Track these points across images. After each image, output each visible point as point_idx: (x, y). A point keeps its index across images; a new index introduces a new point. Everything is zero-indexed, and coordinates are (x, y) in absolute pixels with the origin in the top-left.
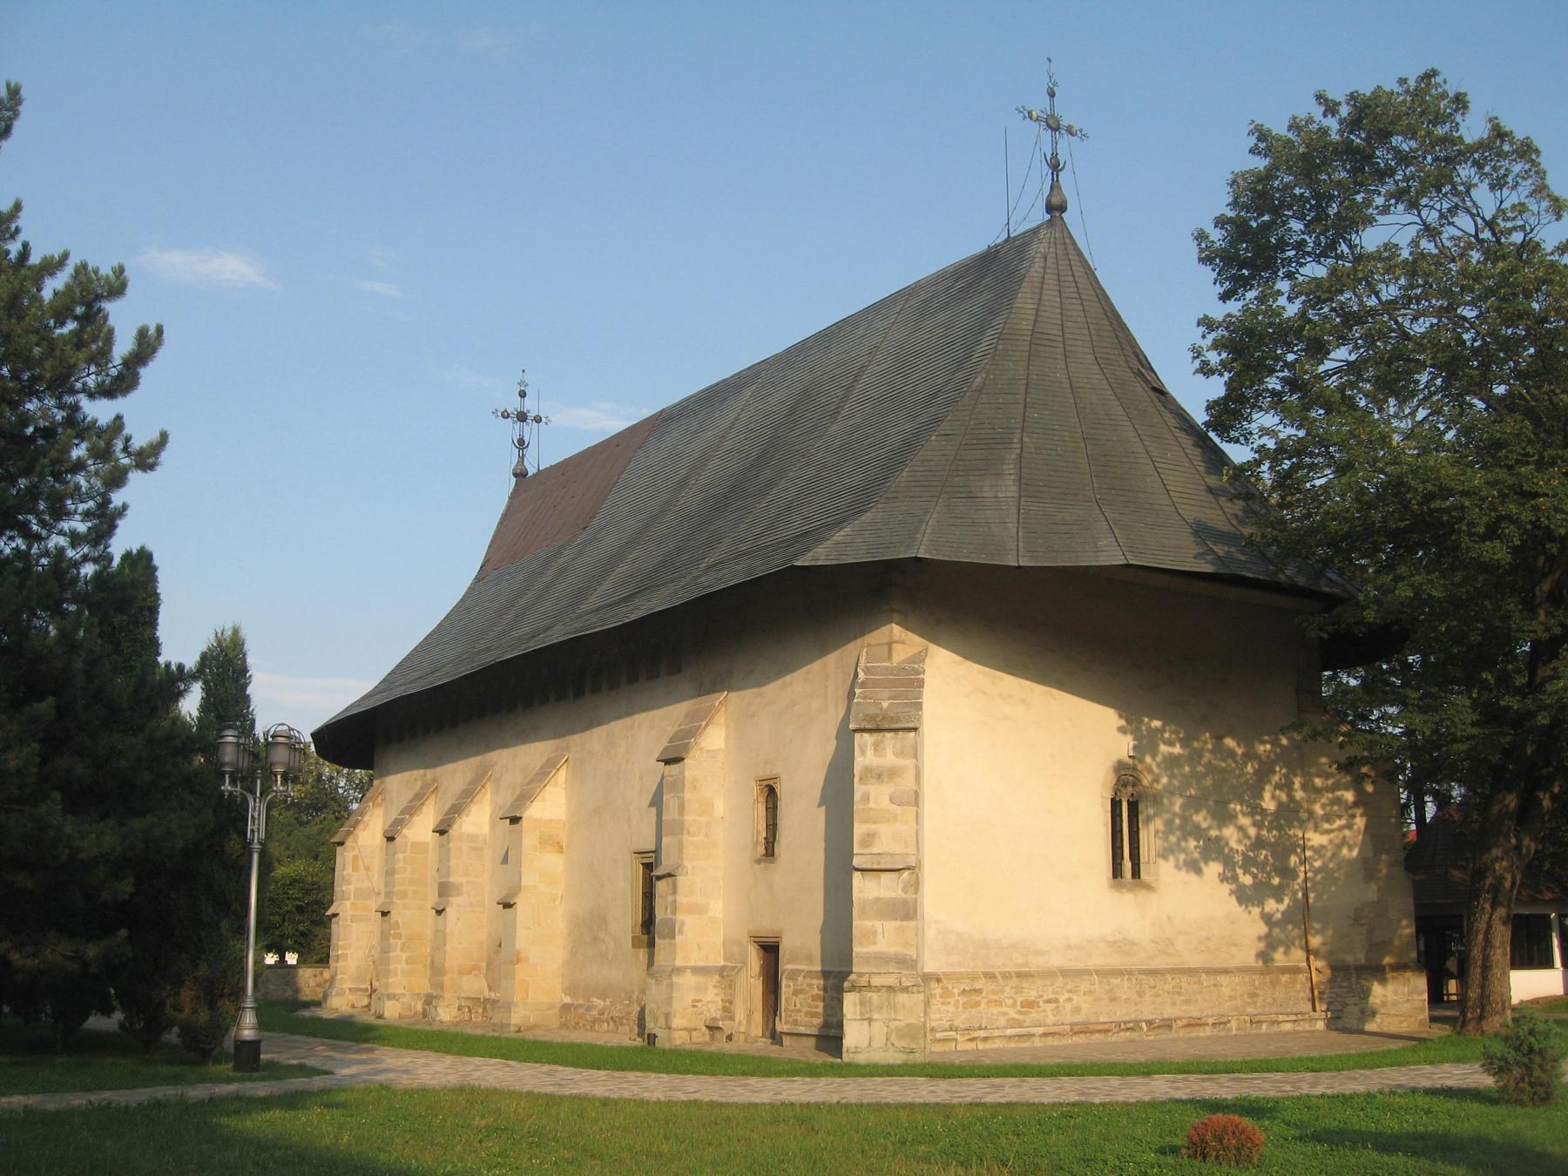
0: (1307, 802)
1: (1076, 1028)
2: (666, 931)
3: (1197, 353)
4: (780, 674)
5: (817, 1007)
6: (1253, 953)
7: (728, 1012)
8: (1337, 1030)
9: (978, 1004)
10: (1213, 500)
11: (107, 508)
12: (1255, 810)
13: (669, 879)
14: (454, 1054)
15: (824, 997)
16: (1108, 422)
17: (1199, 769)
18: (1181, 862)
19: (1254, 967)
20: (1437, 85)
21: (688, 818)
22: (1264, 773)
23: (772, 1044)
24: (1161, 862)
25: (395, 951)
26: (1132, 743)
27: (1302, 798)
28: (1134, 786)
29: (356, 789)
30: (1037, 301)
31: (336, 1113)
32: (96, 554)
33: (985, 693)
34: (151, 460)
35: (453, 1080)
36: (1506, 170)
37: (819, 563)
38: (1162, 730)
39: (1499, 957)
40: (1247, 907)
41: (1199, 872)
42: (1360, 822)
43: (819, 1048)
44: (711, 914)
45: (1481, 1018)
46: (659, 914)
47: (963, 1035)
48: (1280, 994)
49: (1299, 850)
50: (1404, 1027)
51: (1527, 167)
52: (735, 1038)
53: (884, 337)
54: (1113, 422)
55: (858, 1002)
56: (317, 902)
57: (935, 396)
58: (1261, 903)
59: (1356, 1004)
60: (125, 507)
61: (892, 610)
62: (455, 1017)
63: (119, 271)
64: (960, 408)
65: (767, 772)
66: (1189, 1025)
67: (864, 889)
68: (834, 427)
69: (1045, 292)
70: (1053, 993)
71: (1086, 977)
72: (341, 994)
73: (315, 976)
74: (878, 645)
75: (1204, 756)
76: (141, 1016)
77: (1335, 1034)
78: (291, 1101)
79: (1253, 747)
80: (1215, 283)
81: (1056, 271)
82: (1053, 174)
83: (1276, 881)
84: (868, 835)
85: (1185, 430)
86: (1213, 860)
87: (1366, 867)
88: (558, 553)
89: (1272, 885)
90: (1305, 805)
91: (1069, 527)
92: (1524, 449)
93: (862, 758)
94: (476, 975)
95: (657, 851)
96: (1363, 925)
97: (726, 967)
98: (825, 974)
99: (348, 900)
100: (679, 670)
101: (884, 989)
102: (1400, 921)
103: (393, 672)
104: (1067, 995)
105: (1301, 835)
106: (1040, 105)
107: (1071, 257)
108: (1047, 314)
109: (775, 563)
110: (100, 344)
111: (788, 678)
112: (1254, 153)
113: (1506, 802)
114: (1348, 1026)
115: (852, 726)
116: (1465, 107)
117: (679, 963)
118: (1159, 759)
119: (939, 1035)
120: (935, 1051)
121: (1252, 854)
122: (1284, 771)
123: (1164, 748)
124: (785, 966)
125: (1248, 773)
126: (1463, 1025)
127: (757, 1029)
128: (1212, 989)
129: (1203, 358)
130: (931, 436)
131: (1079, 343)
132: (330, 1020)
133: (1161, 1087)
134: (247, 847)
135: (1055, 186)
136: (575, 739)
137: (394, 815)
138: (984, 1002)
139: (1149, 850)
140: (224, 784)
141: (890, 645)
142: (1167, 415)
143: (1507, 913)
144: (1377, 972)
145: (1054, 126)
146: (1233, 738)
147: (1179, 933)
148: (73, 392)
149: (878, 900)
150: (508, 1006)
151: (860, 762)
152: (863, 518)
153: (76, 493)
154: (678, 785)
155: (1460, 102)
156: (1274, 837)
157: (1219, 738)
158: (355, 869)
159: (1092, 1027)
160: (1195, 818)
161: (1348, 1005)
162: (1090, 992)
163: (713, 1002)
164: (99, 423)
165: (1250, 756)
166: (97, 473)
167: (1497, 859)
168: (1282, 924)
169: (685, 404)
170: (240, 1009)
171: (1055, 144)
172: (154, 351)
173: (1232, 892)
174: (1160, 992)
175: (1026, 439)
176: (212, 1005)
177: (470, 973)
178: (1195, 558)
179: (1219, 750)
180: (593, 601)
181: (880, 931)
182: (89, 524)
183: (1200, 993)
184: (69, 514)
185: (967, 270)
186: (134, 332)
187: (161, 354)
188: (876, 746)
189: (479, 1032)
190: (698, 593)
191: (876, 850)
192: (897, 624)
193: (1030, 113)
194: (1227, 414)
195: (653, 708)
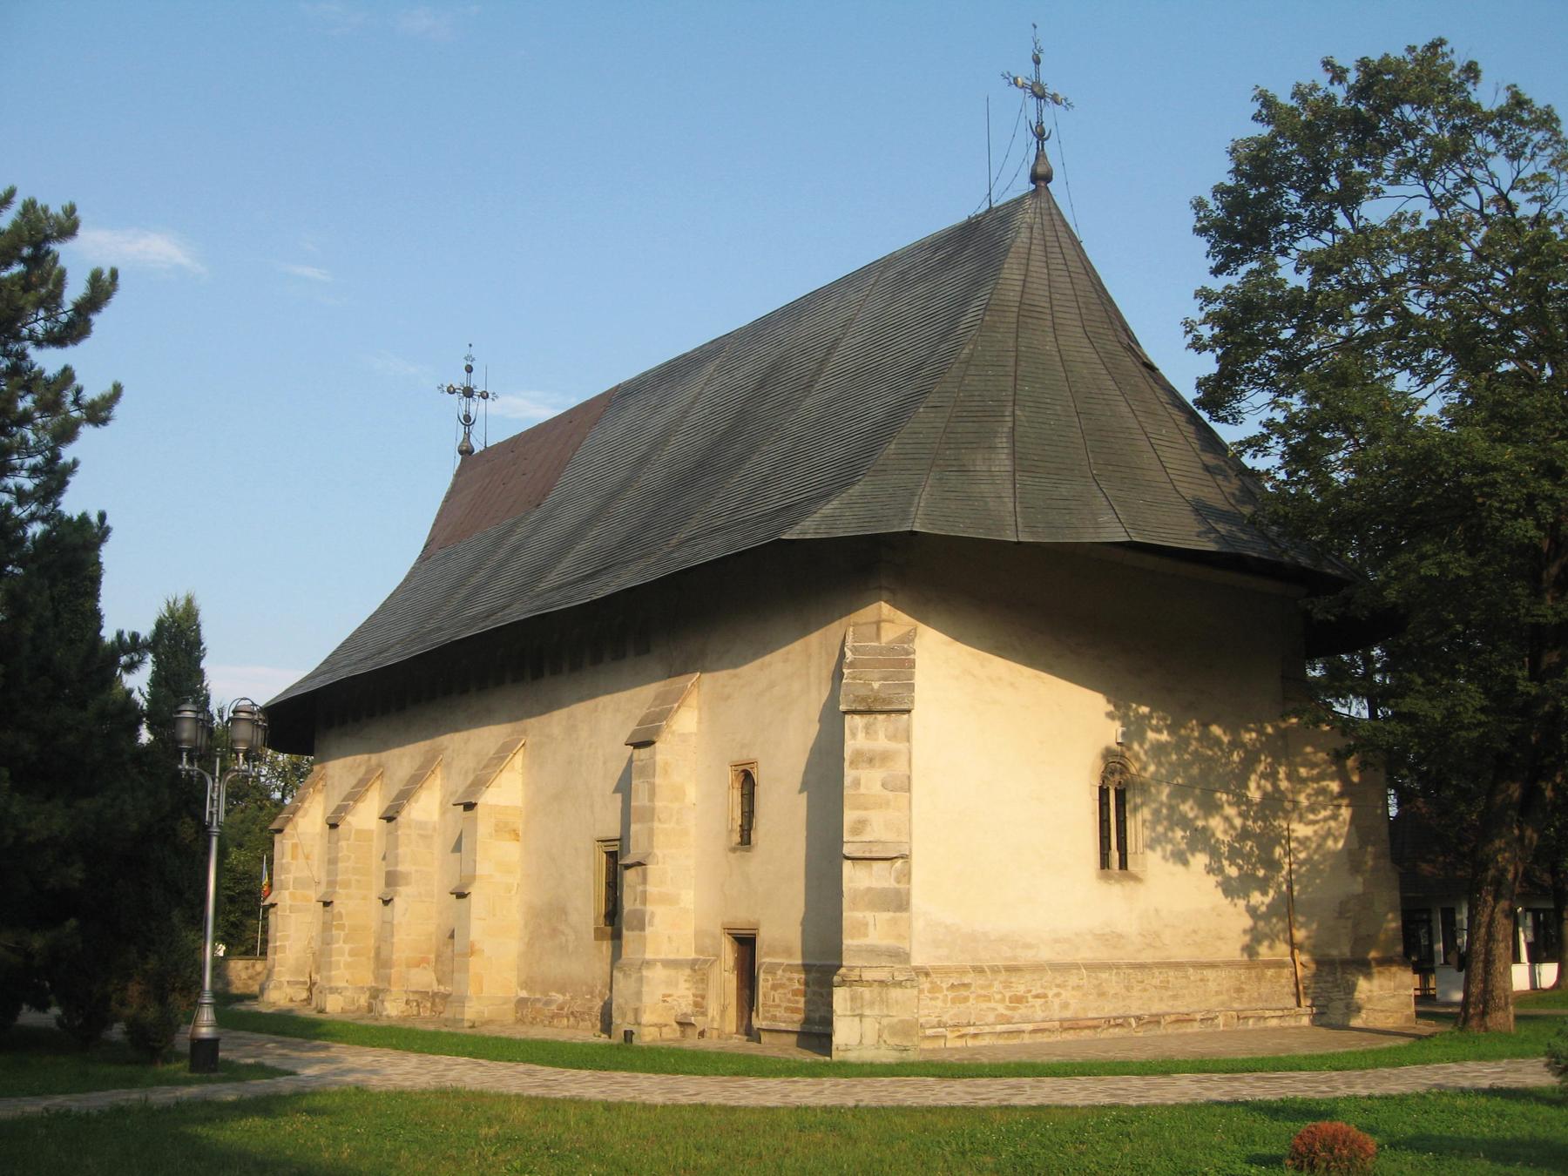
0: (1292, 792)
1: (1066, 1025)
3: (1189, 327)
4: (757, 655)
5: (797, 1002)
6: (1239, 946)
7: (700, 1006)
8: (1321, 1025)
9: (966, 999)
10: (1209, 478)
11: (56, 464)
12: (1241, 800)
13: (639, 868)
14: (415, 1051)
15: (805, 992)
17: (1186, 756)
18: (1168, 853)
19: (1240, 961)
20: (1444, 55)
21: (659, 804)
23: (748, 1040)
24: (1149, 852)
25: (338, 942)
26: (1120, 730)
27: (1287, 789)
28: (1121, 773)
29: (279, 776)
30: (1023, 272)
31: (324, 1121)
32: (45, 513)
33: (974, 676)
34: (103, 414)
36: (1527, 138)
37: (808, 537)
39: (1502, 951)
40: (1232, 899)
41: (1185, 863)
42: (1345, 813)
43: (800, 1044)
44: (682, 905)
45: (1484, 1014)
46: (628, 904)
47: (952, 1031)
48: (1265, 989)
49: (1283, 842)
50: (1389, 1023)
51: (1547, 136)
52: (707, 1035)
54: (1106, 397)
55: (848, 996)
56: (249, 892)
57: (919, 367)
58: (1246, 896)
59: (1341, 999)
60: (75, 463)
61: (880, 588)
62: (403, 1012)
63: (71, 211)
64: (949, 380)
65: (744, 756)
66: (1177, 1021)
67: (854, 878)
68: (809, 400)
69: (1031, 263)
70: (1042, 987)
71: (1075, 971)
72: (279, 987)
73: (247, 968)
74: (865, 624)
75: (1191, 744)
76: (81, 1012)
77: (1323, 1030)
78: (266, 1106)
79: (1239, 734)
80: (1207, 256)
81: (1043, 243)
82: (1038, 143)
83: (1261, 873)
84: (859, 822)
85: (1178, 407)
86: (1200, 851)
87: (1352, 859)
88: (510, 531)
89: (1258, 877)
90: (1290, 796)
91: (1067, 502)
92: (1553, 424)
93: (853, 742)
94: (425, 968)
95: (624, 839)
96: (1348, 918)
97: (698, 959)
98: (807, 968)
100: (648, 651)
101: (876, 984)
102: (1386, 914)
103: (335, 653)
104: (1055, 990)
105: (1285, 826)
106: (1025, 72)
108: (1035, 286)
109: (759, 537)
110: (51, 287)
111: (768, 658)
113: (1510, 792)
114: (1333, 1022)
115: (843, 708)
116: (1476, 77)
117: (649, 956)
118: (1147, 746)
119: (929, 1032)
120: (920, 1049)
121: (1237, 845)
122: (1269, 760)
123: (1151, 735)
124: (763, 959)
126: (1466, 1020)
127: (731, 1023)
128: (1199, 983)
129: (1196, 333)
130: (918, 407)
132: (266, 1014)
133: (1184, 1089)
134: (203, 830)
135: (1040, 155)
136: (533, 722)
137: (336, 801)
138: (972, 997)
139: (1136, 840)
140: (181, 764)
141: (878, 623)
142: (1160, 392)
143: (1510, 905)
144: (1363, 966)
145: (1039, 94)
146: (1220, 726)
147: (1166, 926)
148: (18, 338)
149: (869, 889)
150: (462, 1000)
151: (851, 745)
153: (24, 448)
154: (649, 770)
155: (1472, 71)
156: (1260, 827)
157: (1205, 725)
159: (1082, 1023)
162: (1078, 987)
163: (683, 997)
164: (46, 374)
165: (1236, 744)
166: (44, 427)
168: (1266, 917)
170: (196, 1005)
171: (1040, 112)
172: (108, 295)
173: (1218, 884)
174: (1148, 986)
175: (1018, 413)
177: (418, 966)
179: (1206, 738)
180: (553, 579)
181: (871, 922)
182: (37, 481)
184: (14, 470)
186: (88, 275)
187: (116, 300)
188: (867, 728)
189: (431, 1028)
190: (673, 569)
192: (886, 602)
193: (1015, 79)
194: (1218, 393)
195: (618, 690)
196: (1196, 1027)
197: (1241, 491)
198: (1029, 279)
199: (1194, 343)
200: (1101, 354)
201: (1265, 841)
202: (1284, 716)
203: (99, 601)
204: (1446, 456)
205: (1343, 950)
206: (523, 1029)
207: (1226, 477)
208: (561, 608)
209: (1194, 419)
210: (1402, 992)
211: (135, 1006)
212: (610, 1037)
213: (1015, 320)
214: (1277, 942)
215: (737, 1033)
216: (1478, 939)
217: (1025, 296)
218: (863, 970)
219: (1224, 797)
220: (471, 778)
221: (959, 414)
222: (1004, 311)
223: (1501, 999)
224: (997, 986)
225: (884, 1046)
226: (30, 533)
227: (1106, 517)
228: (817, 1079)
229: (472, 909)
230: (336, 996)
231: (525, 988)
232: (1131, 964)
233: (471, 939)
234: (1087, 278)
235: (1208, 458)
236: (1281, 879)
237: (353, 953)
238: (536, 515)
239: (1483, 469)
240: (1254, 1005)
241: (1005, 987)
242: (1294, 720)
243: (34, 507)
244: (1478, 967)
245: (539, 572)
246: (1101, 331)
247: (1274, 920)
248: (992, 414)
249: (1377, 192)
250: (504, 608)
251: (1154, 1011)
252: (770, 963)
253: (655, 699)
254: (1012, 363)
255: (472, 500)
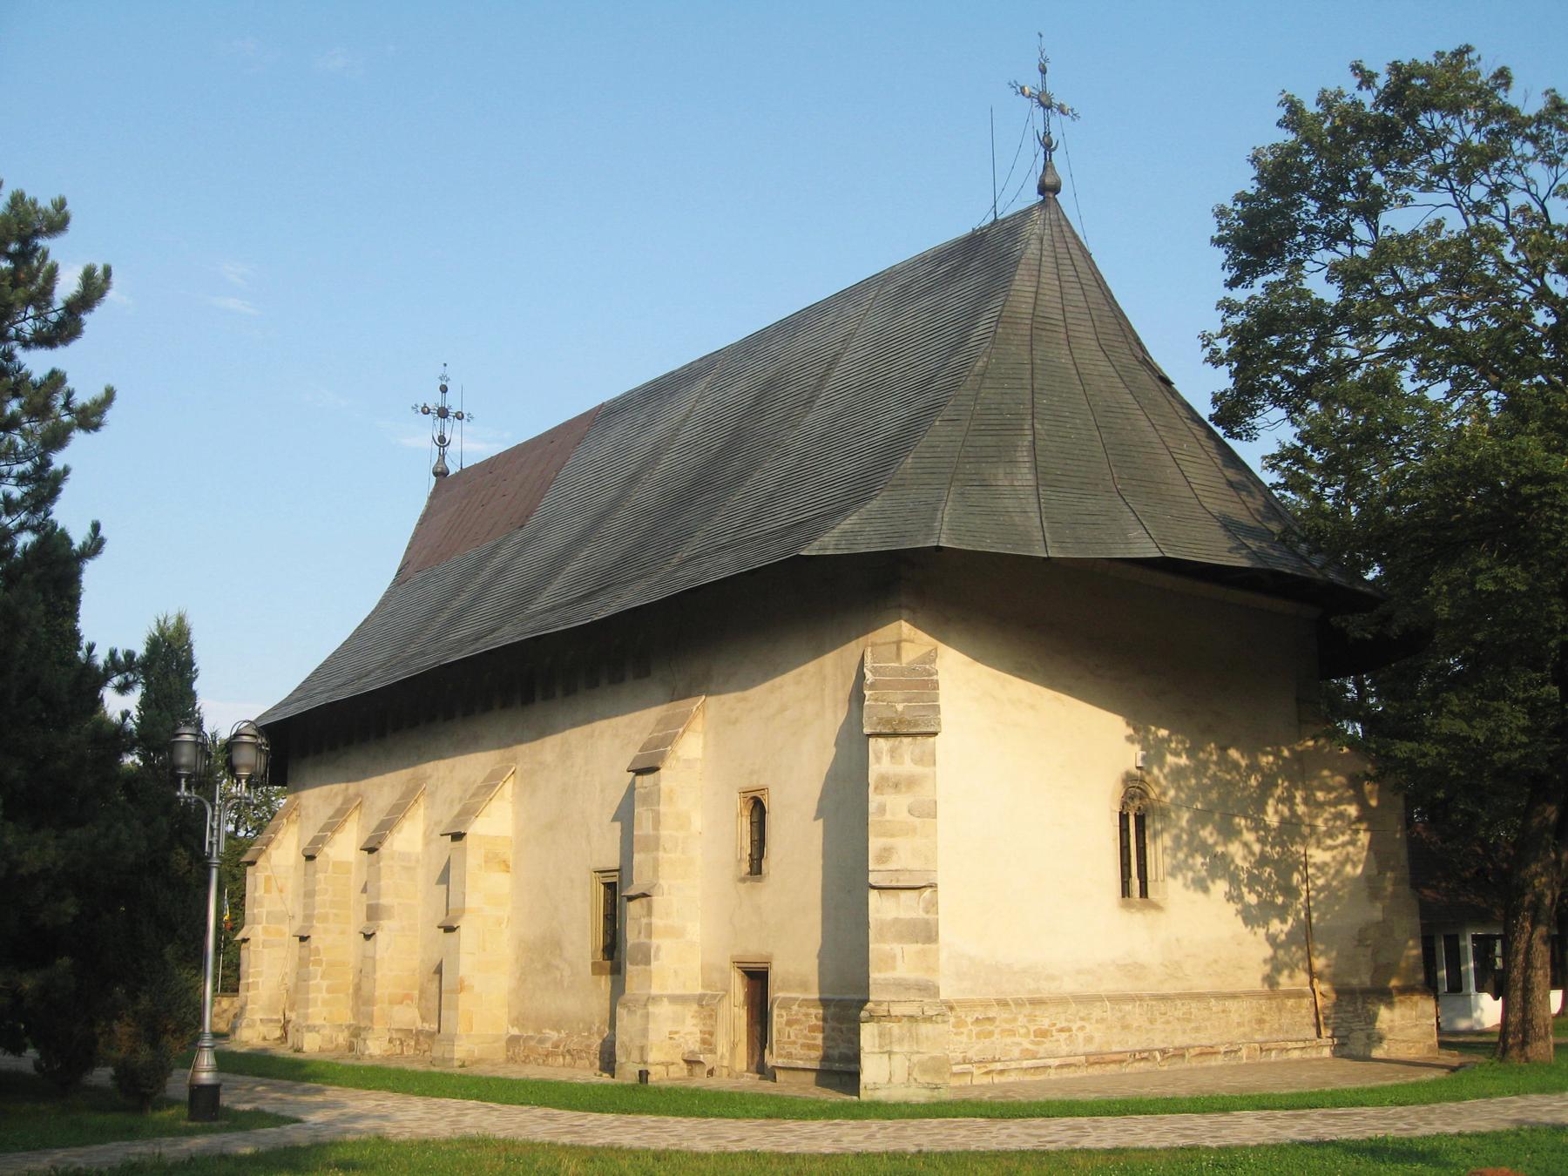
0: (1310, 817)
1: (1092, 1059)
2: (640, 956)
3: (1207, 340)
4: (767, 676)
5: (814, 1039)
6: (1259, 977)
7: (708, 1044)
8: (1342, 1056)
9: (991, 1034)
10: (1234, 494)
12: (1259, 825)
13: (644, 900)
15: (823, 1028)
16: (1120, 410)
20: (1470, 63)
21: (664, 832)
22: (1267, 787)
23: (760, 1079)
24: (1169, 880)
25: (315, 978)
26: (1140, 753)
27: (1304, 813)
30: (1035, 284)
32: (36, 522)
34: (95, 420)
37: (828, 553)
38: (1168, 740)
40: (1252, 928)
41: (1206, 890)
42: (1364, 838)
43: (819, 1083)
45: (1524, 1043)
46: (632, 937)
48: (1286, 1019)
49: (1301, 868)
50: (1412, 1054)
52: (716, 1073)
53: (859, 324)
54: (1125, 411)
57: (930, 380)
60: (66, 471)
61: (900, 606)
63: (61, 205)
64: (965, 393)
65: (755, 782)
66: (1201, 1054)
67: (880, 908)
68: (810, 417)
69: (1043, 274)
70: (1066, 1020)
71: (1098, 1004)
72: (251, 1026)
74: (884, 644)
75: (1209, 768)
79: (1257, 758)
80: (1223, 268)
82: (1045, 153)
83: (1280, 900)
86: (1220, 878)
87: (1371, 885)
90: (1307, 820)
93: (877, 766)
94: (408, 1005)
96: (1368, 946)
97: (705, 995)
98: (824, 1003)
99: (260, 924)
100: (622, 679)
101: (906, 1019)
102: (1407, 942)
103: (308, 679)
104: (1079, 1023)
105: (1303, 852)
106: (1032, 82)
107: (1068, 240)
108: (1047, 297)
109: (774, 554)
111: (778, 681)
112: (1281, 126)
113: (1546, 815)
114: (1354, 1053)
115: (867, 730)
117: (655, 991)
118: (1166, 770)
119: (956, 1069)
121: (1256, 872)
122: (1286, 784)
123: (1170, 759)
124: (776, 993)
125: (1252, 787)
126: (1505, 1051)
127: (742, 1061)
129: (1214, 347)
131: (1082, 328)
135: (1048, 166)
136: (523, 749)
138: (997, 1031)
140: (180, 791)
141: (898, 643)
143: (1547, 931)
144: (1385, 996)
146: (1237, 749)
148: (8, 339)
149: (896, 920)
150: (451, 1040)
151: (875, 770)
152: (868, 506)
154: (653, 798)
155: (1503, 76)
156: (1278, 853)
157: (1223, 749)
158: (267, 891)
159: (1108, 1058)
160: (1201, 833)
161: (1355, 1031)
162: (1101, 1020)
163: (691, 1033)
165: (1254, 767)
167: (1536, 874)
169: (630, 396)
172: (101, 293)
173: (1238, 912)
174: (1171, 1018)
175: (1037, 426)
176: (154, 1043)
177: (401, 1003)
178: (1229, 552)
179: (1224, 761)
180: (544, 600)
182: (25, 489)
183: (1209, 1019)
185: (950, 254)
189: (419, 1067)
190: (679, 588)
192: (906, 621)
193: (1022, 88)
196: (1218, 1061)
197: (1265, 507)
198: (1041, 291)
199: (1211, 357)
200: (1118, 368)
201: (1283, 866)
202: (1301, 737)
203: (78, 621)
204: (1505, 466)
205: (1364, 979)
206: (516, 1068)
207: (1250, 493)
208: (559, 629)
209: (1212, 434)
210: (1424, 1021)
211: (124, 1050)
212: (613, 1077)
213: (1029, 333)
214: (1297, 970)
215: (748, 1070)
216: (1515, 966)
217: (1038, 308)
218: (891, 1004)
219: (1243, 822)
220: (457, 809)
221: (977, 427)
222: (1017, 323)
223: (1540, 1028)
224: (1021, 1020)
225: (914, 1083)
226: (20, 545)
227: (1136, 533)
228: (859, 1122)
229: (461, 945)
230: (314, 1034)
231: (517, 1026)
232: (1153, 995)
233: (461, 974)
234: (1099, 290)
235: (1231, 474)
236: (1299, 906)
237: (330, 990)
238: (518, 537)
239: (1540, 478)
240: (1274, 1036)
241: (1029, 1021)
242: (1311, 743)
243: (23, 517)
244: (1517, 996)
245: (528, 593)
246: (1116, 344)
247: (1294, 949)
248: (1011, 427)
249: (1405, 200)
250: (493, 631)
251: (1177, 1044)
252: (784, 999)
253: (657, 724)
254: (1028, 376)
255: (449, 522)
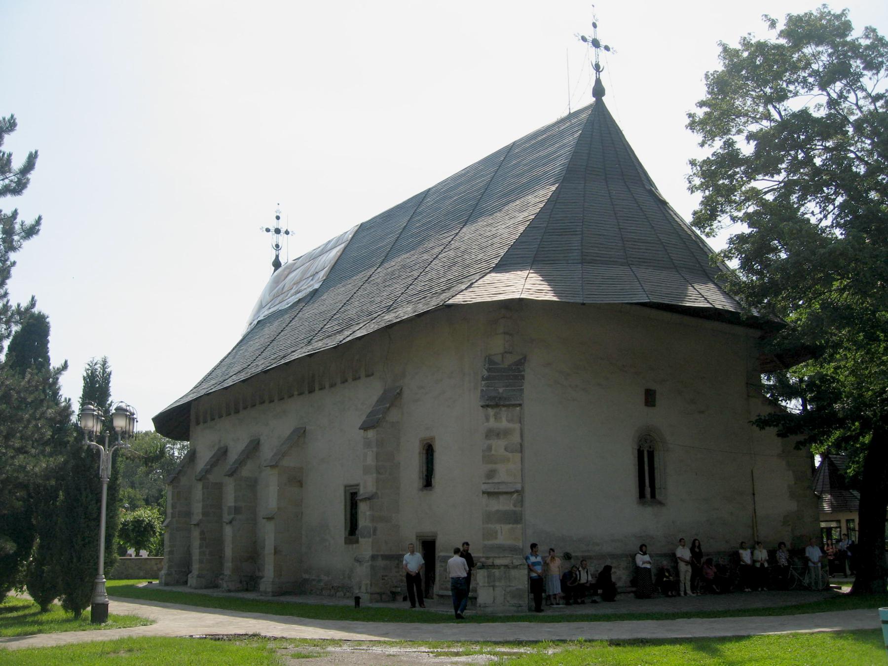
35: (117, 637)
55: (486, 574)
149: (497, 511)
191: (496, 481)
